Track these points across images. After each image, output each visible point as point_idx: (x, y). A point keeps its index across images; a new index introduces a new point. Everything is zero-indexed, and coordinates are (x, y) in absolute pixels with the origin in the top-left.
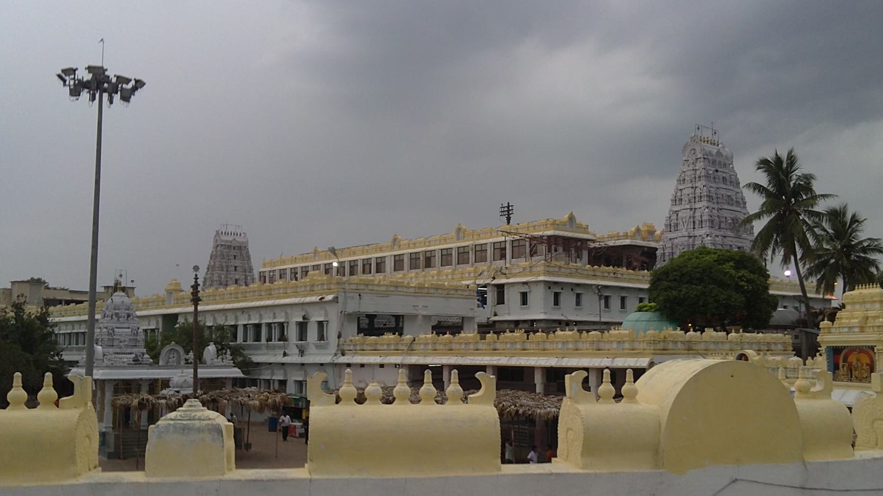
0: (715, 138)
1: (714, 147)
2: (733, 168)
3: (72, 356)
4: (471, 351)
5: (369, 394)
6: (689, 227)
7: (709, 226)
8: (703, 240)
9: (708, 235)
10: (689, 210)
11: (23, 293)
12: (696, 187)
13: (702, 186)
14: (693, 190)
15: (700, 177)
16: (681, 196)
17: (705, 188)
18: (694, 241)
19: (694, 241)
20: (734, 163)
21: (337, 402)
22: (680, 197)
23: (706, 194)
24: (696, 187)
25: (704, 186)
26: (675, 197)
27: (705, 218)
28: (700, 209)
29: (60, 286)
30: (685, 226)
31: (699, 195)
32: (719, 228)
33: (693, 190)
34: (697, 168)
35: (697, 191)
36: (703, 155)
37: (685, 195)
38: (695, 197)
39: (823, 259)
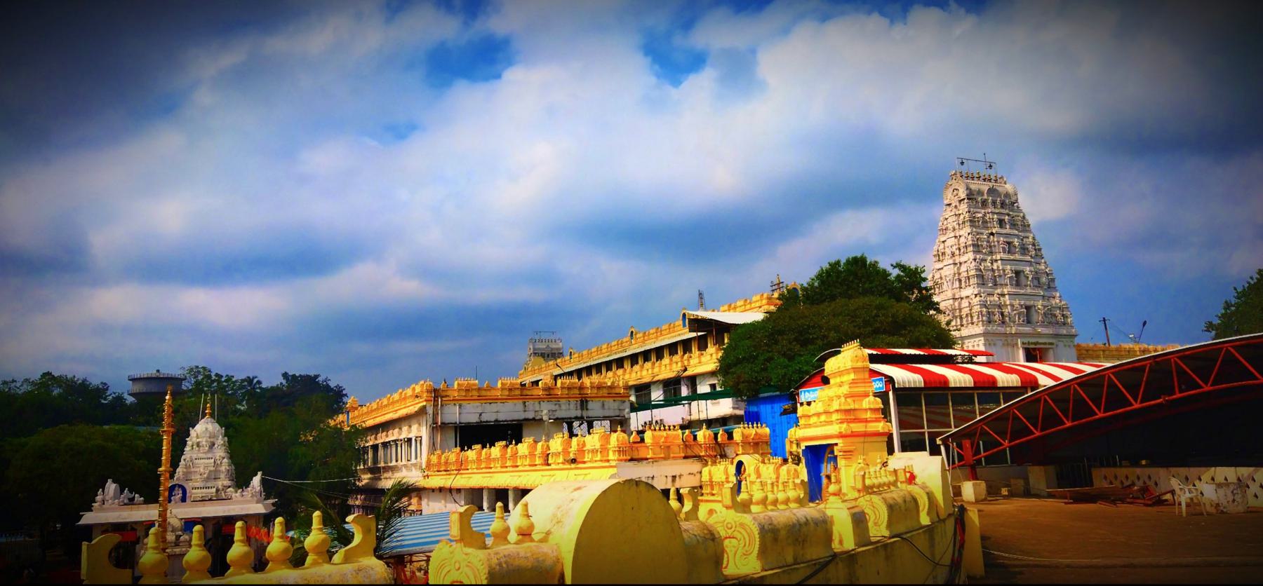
0: (992, 173)
1: (985, 183)
2: (1018, 207)
3: (382, 417)
4: (509, 469)
5: (231, 561)
6: (954, 287)
7: (977, 284)
8: (971, 301)
9: (976, 295)
10: (952, 266)
11: (230, 374)
12: (960, 236)
13: (967, 234)
14: (956, 240)
15: (964, 223)
16: (944, 249)
17: (970, 236)
18: (960, 304)
19: (960, 304)
20: (1019, 201)
21: (165, 573)
22: (943, 251)
23: (971, 242)
24: (960, 236)
25: (969, 234)
26: (938, 251)
27: (973, 273)
28: (966, 264)
29: (167, 372)
30: (950, 287)
31: (964, 245)
32: (1049, 288)
33: (956, 240)
34: (960, 212)
35: (961, 242)
36: (967, 195)
37: (948, 247)
38: (960, 249)
39: (13, 540)
